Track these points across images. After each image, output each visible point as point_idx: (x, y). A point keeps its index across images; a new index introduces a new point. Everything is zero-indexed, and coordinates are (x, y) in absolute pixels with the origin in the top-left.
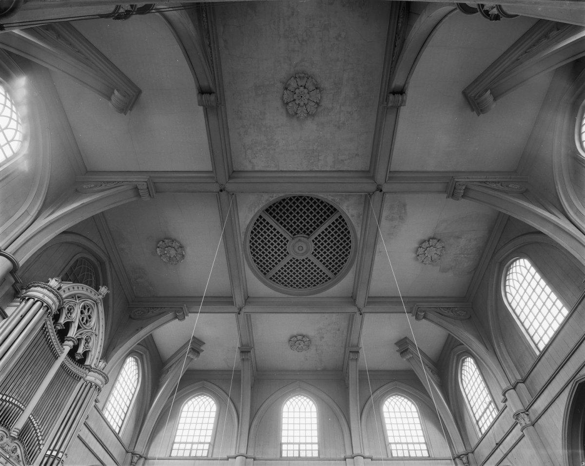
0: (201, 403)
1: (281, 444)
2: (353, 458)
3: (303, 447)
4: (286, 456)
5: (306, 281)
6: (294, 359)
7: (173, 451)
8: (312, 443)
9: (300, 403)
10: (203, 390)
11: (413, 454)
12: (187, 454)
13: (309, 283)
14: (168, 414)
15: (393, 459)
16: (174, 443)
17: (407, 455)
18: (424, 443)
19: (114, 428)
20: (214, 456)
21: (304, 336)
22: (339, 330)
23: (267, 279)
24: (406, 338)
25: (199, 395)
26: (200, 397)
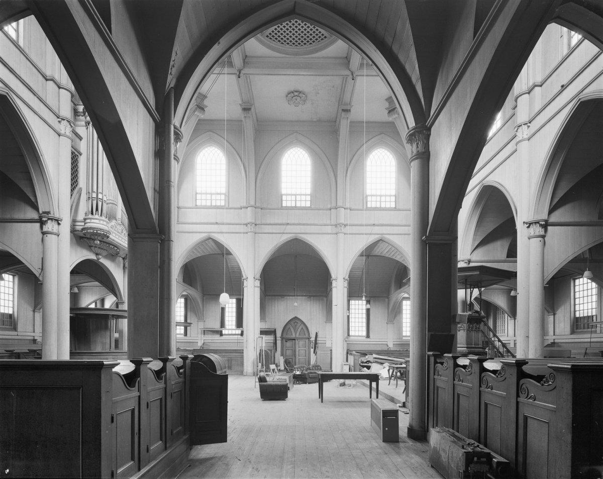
1: (282, 196)
5: (302, 39)
6: (289, 111)
7: (197, 201)
8: (306, 195)
10: (211, 141)
11: (383, 205)
12: (209, 204)
13: (305, 42)
15: (368, 209)
16: (196, 193)
17: (378, 206)
18: (394, 196)
20: (230, 206)
21: (300, 92)
22: (333, 87)
23: (264, 37)
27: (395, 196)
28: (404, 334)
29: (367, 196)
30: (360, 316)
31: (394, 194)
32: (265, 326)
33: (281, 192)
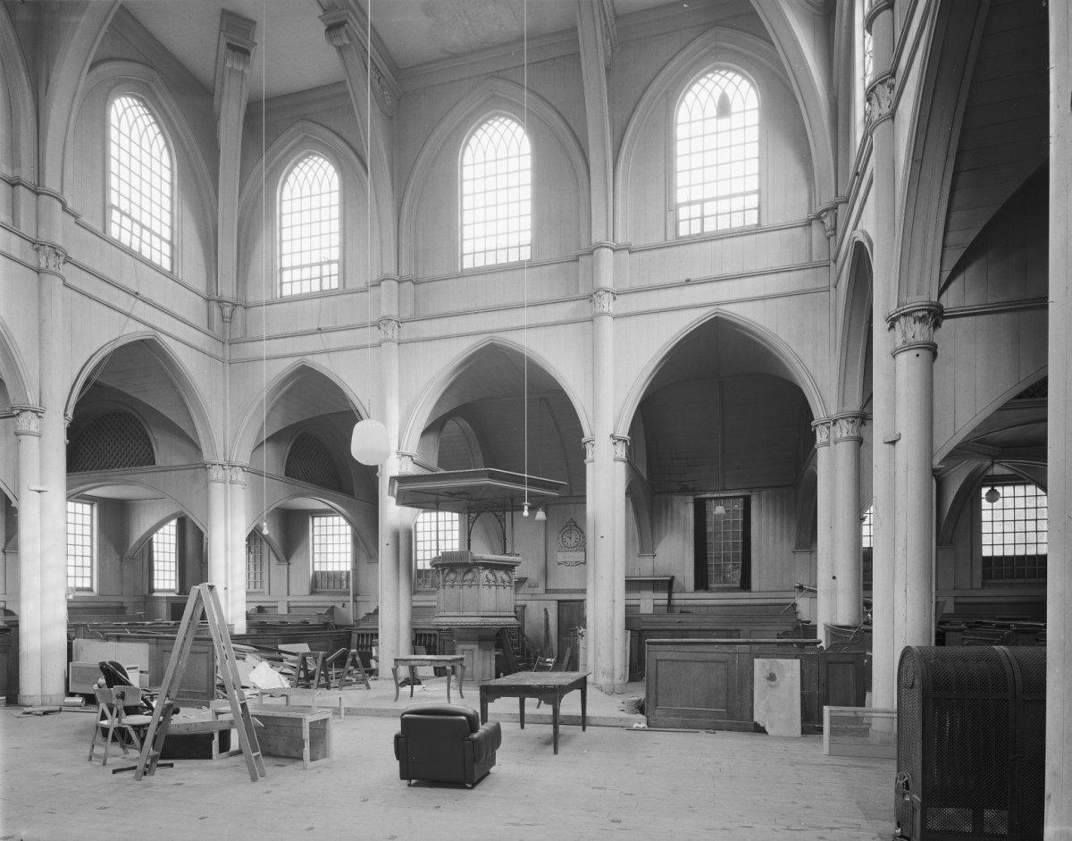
0: (496, 137)
2: (592, 253)
3: (710, 208)
4: (471, 266)
9: (321, 173)
11: (710, 227)
14: (255, 218)
15: (283, 300)
19: (158, 262)
24: (254, 23)
25: (488, 119)
26: (490, 122)
27: (759, 192)
28: (158, 585)
29: (677, 206)
30: (343, 540)
31: (757, 188)
32: (646, 568)
33: (676, 200)
